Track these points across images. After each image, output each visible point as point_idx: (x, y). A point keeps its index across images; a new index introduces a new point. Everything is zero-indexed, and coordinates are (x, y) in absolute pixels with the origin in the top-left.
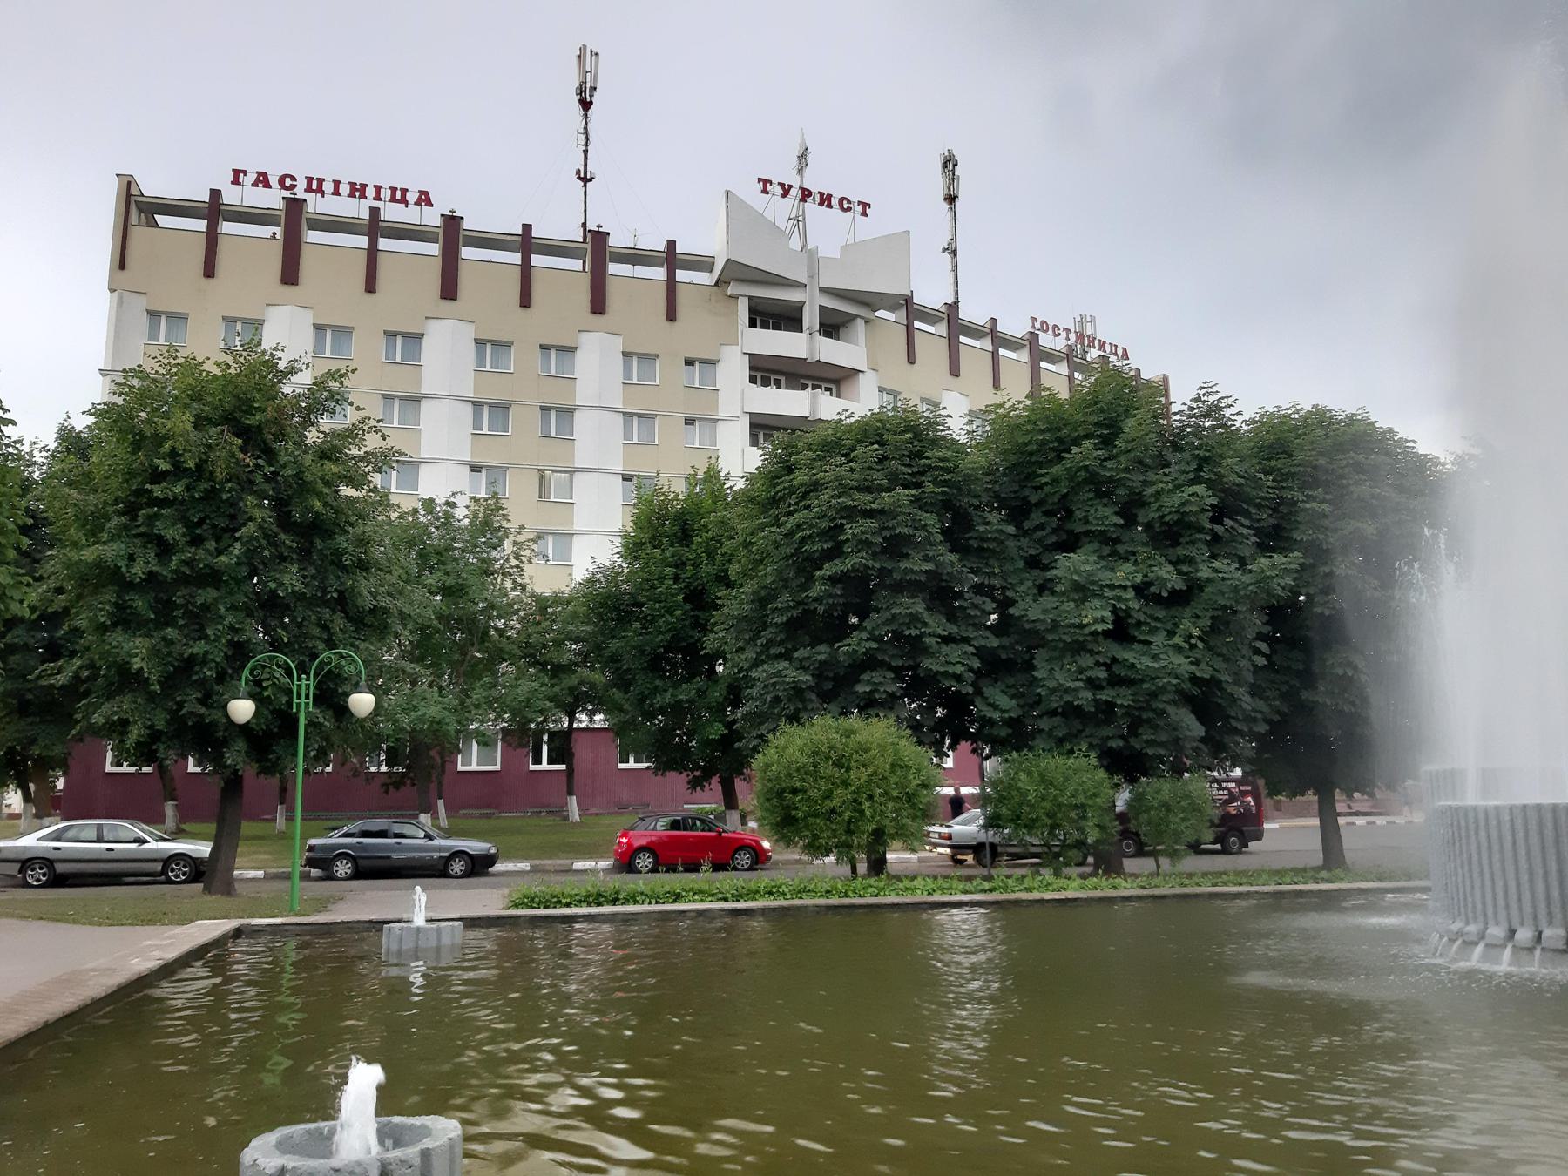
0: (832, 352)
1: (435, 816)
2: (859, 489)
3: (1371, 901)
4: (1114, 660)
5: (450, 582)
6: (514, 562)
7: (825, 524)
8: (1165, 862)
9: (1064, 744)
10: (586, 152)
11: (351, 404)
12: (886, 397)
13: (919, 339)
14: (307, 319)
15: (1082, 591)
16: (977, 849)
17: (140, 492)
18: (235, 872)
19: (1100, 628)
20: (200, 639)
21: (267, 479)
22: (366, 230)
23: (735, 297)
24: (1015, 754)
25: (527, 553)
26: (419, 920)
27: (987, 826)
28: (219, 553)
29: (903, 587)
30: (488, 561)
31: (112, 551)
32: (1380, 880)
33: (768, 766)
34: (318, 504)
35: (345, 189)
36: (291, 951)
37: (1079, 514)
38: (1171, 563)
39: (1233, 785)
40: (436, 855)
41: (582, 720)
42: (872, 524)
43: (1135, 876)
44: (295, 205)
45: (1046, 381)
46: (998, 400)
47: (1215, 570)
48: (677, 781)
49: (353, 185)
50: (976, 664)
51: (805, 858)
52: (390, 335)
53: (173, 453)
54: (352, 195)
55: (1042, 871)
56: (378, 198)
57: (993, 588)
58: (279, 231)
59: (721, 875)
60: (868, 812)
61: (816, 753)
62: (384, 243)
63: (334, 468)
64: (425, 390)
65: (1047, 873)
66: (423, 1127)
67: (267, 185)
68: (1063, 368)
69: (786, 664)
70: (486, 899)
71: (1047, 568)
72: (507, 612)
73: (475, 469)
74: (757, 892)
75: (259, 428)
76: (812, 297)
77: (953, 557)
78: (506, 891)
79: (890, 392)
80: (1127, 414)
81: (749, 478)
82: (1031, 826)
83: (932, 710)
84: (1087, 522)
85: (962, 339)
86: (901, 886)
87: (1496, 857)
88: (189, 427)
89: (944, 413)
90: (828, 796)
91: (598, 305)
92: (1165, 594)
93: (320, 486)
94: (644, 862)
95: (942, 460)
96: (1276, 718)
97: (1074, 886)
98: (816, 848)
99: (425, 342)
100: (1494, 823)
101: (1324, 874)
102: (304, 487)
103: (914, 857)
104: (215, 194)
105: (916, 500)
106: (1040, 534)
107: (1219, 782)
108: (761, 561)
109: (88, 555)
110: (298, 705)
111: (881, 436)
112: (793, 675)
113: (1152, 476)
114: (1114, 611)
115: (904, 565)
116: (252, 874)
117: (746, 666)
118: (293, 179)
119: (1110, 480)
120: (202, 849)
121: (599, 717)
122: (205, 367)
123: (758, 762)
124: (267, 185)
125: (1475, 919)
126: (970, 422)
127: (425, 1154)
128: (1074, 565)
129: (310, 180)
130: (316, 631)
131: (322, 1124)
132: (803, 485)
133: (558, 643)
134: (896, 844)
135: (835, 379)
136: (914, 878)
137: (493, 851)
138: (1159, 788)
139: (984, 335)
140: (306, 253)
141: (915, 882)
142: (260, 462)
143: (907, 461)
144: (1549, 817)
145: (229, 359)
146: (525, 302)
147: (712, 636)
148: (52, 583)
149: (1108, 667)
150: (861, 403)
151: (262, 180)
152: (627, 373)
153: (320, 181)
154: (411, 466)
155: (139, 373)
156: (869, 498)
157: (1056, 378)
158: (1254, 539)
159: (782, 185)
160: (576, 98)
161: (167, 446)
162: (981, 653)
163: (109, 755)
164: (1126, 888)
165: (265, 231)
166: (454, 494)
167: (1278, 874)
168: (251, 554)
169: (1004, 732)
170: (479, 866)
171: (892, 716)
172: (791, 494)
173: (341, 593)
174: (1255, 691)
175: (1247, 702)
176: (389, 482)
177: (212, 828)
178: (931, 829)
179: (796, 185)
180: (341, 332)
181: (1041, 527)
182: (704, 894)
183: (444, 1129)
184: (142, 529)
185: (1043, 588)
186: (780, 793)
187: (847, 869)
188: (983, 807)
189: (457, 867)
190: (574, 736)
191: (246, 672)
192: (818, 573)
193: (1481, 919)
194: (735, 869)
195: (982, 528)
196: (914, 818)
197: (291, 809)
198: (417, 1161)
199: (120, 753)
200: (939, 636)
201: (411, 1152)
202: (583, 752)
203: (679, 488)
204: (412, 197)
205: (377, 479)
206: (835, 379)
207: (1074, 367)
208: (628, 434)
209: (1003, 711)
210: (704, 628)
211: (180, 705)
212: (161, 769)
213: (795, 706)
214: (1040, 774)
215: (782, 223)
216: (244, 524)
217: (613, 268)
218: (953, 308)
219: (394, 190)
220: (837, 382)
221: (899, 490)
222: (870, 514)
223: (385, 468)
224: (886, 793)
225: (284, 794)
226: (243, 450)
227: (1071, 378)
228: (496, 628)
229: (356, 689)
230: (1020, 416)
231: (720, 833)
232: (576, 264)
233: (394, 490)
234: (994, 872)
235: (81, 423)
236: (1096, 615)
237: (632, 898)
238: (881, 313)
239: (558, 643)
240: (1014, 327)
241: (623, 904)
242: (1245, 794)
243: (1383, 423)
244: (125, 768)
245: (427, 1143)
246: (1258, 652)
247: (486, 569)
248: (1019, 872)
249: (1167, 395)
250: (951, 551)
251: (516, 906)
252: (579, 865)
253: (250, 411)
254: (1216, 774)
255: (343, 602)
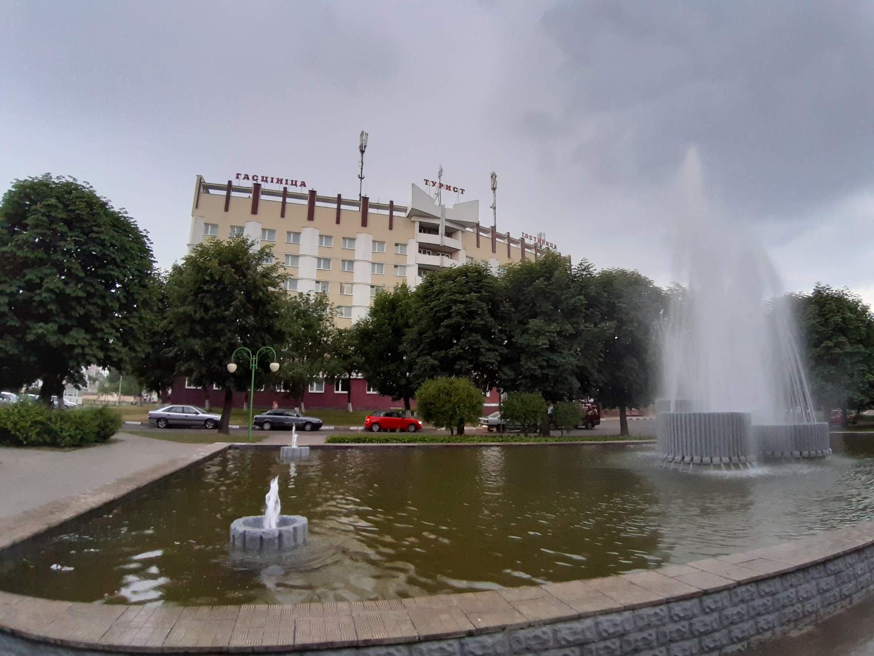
0: (449, 242)
1: (300, 409)
2: (458, 293)
3: (638, 447)
4: (549, 359)
5: (307, 323)
6: (330, 316)
7: (445, 306)
8: (565, 432)
9: (530, 389)
10: (362, 168)
11: (274, 257)
12: (468, 259)
13: (481, 238)
14: (259, 227)
15: (538, 333)
16: (498, 426)
17: (200, 288)
18: (230, 426)
19: (544, 347)
20: (218, 341)
21: (244, 284)
22: (282, 194)
23: (414, 222)
24: (512, 392)
25: (335, 312)
26: (294, 446)
27: (502, 417)
28: (226, 310)
29: (476, 330)
30: (321, 316)
31: (189, 309)
32: (640, 439)
33: (422, 394)
34: (261, 294)
35: (275, 181)
36: (249, 454)
37: (538, 305)
38: (570, 323)
39: (590, 405)
40: (300, 422)
41: (354, 375)
42: (462, 306)
43: (554, 437)
44: (257, 186)
45: (527, 255)
46: (510, 262)
47: (586, 327)
48: (388, 399)
49: (278, 179)
50: (499, 359)
51: (434, 428)
52: (289, 233)
53: (211, 274)
54: (277, 182)
55: (521, 434)
56: (286, 183)
57: (506, 331)
58: (251, 195)
59: (403, 433)
60: (458, 412)
61: (439, 390)
62: (288, 200)
63: (267, 280)
64: (300, 253)
65: (522, 435)
66: (294, 519)
67: (248, 179)
68: (533, 251)
69: (429, 357)
70: (319, 440)
71: (525, 324)
72: (328, 335)
73: (317, 282)
74: (417, 440)
75: (241, 266)
76: (442, 223)
77: (491, 319)
78: (325, 437)
79: (470, 258)
80: (556, 269)
81: (418, 288)
82: (517, 419)
83: (482, 376)
84: (541, 308)
85: (497, 239)
86: (469, 439)
87: (679, 431)
88: (217, 265)
89: (490, 266)
90: (443, 406)
91: (364, 223)
92: (568, 335)
93: (262, 287)
94: (376, 428)
95: (488, 283)
96: (606, 381)
97: (532, 440)
98: (438, 425)
99: (357, 242)
100: (679, 419)
101: (621, 437)
102: (256, 288)
103: (475, 428)
104: (230, 182)
105: (479, 298)
106: (524, 311)
107: (585, 403)
108: (421, 318)
109: (181, 310)
110: (252, 367)
111: (466, 274)
112: (431, 361)
113: (565, 292)
114: (550, 341)
115: (474, 322)
116: (235, 427)
117: (414, 357)
118: (257, 177)
119: (549, 293)
120: (218, 417)
121: (360, 374)
122: (223, 243)
123: (417, 393)
124: (248, 179)
125: (671, 453)
126: (499, 270)
127: (295, 529)
128: (534, 323)
129: (263, 177)
130: (259, 340)
131: (259, 516)
132: (437, 290)
133: (346, 347)
134: (469, 424)
135: (450, 252)
136: (474, 437)
137: (321, 422)
138: (563, 406)
139: (505, 238)
140: (260, 203)
141: (475, 438)
142: (241, 278)
143: (476, 283)
144: (698, 417)
145: (231, 241)
146: (338, 222)
147: (402, 345)
148: (168, 320)
149: (547, 361)
150: (459, 262)
151: (247, 177)
152: (374, 248)
153: (267, 178)
154: (295, 281)
155: (201, 245)
156: (461, 296)
157: (530, 255)
158: (600, 316)
159: (433, 182)
160: (359, 150)
161: (209, 271)
162: (501, 355)
163: (187, 382)
164: (551, 442)
165: (246, 195)
166: (310, 291)
167: (605, 438)
168: (237, 310)
169: (509, 384)
170: (316, 427)
171: (468, 378)
172: (432, 294)
173: (268, 326)
174: (599, 372)
175: (596, 375)
176: (287, 286)
177: (222, 410)
178: (481, 418)
179: (438, 182)
180: (272, 232)
181: (524, 309)
182: (398, 440)
183: (301, 521)
184: (199, 301)
185: (525, 332)
186: (426, 404)
187: (449, 433)
188: (500, 411)
189: (308, 427)
190: (352, 381)
191: (234, 354)
192: (442, 324)
193: (673, 454)
194: (409, 431)
195: (503, 309)
196: (475, 414)
197: (249, 404)
198: (292, 530)
199: (190, 381)
200: (486, 348)
201: (290, 528)
202: (354, 388)
203: (392, 291)
204: (299, 183)
205: (282, 285)
206: (450, 252)
207: (537, 251)
208: (373, 270)
209: (509, 376)
210: (400, 343)
211: (211, 365)
212: (204, 388)
213: (432, 371)
214: (521, 400)
215: (432, 195)
216: (234, 300)
217: (370, 210)
218: (494, 228)
219: (292, 181)
220: (451, 254)
221: (473, 294)
222: (462, 302)
223: (285, 280)
224: (465, 405)
225: (247, 398)
226: (235, 273)
227: (536, 255)
228: (323, 340)
229: (273, 362)
230: (517, 268)
231: (403, 418)
232: (357, 209)
233: (288, 289)
234: (503, 435)
235: (181, 263)
236: (543, 342)
237: (371, 441)
238: (468, 229)
239: (346, 347)
240: (516, 236)
241: (368, 443)
242: (594, 408)
243: (643, 275)
244: (192, 387)
245: (295, 525)
246: (601, 357)
247: (320, 319)
248: (512, 435)
249: (570, 263)
250: (491, 317)
251: (329, 442)
252: (352, 428)
253: (239, 259)
254: (584, 401)
255: (269, 329)
